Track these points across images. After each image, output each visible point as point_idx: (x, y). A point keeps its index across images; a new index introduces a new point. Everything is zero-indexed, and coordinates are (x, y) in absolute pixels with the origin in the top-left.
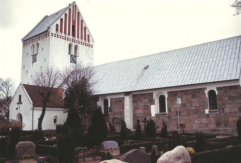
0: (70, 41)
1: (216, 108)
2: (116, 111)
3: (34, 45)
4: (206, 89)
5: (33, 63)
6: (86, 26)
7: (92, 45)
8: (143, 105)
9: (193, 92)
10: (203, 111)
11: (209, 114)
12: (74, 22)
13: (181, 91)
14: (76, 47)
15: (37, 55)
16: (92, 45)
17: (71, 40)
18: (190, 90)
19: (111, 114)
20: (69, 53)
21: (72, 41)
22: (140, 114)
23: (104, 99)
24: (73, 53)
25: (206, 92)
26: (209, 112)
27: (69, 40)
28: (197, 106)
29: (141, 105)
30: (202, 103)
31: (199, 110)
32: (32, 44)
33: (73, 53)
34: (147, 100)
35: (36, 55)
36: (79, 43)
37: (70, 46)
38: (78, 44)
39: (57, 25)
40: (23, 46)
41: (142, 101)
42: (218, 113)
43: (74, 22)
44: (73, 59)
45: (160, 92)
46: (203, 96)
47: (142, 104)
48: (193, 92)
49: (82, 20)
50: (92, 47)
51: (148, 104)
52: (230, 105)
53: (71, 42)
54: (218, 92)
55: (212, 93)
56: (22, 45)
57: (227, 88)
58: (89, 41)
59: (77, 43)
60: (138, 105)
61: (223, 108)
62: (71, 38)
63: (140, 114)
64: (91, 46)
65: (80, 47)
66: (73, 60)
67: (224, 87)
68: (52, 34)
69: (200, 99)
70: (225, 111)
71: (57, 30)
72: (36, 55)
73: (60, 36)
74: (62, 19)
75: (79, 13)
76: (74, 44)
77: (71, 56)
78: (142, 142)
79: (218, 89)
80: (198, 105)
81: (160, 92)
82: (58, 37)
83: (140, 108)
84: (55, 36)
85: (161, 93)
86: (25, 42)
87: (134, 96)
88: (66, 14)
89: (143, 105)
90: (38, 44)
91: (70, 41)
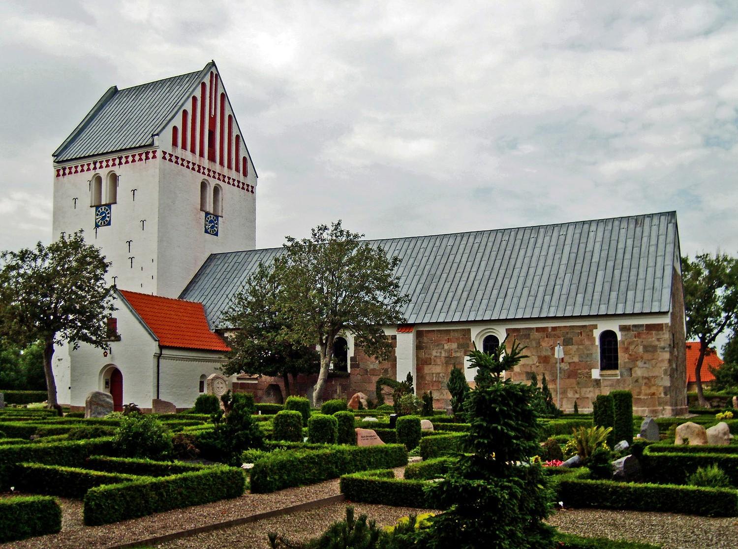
0: (204, 173)
1: (615, 367)
2: (372, 367)
3: (99, 180)
4: (595, 327)
5: (97, 226)
6: (239, 134)
7: (252, 187)
8: (443, 355)
9: (567, 333)
10: (587, 373)
11: (600, 380)
12: (213, 121)
13: (538, 329)
14: (216, 190)
15: (113, 206)
16: (252, 187)
17: (206, 172)
18: (559, 327)
19: (356, 372)
20: (202, 210)
21: (209, 175)
22: (434, 375)
23: (485, 336)
24: (210, 208)
25: (597, 334)
26: (601, 375)
27: (202, 171)
28: (574, 362)
29: (438, 354)
30: (584, 357)
31: (579, 371)
32: (92, 173)
33: (210, 208)
34: (454, 346)
35: (109, 205)
36: (224, 181)
37: (204, 186)
38: (221, 183)
39: (175, 129)
40: (58, 175)
41: (439, 345)
42: (619, 378)
43: (213, 121)
44: (212, 225)
45: (487, 329)
46: (587, 343)
47: (441, 353)
48: (567, 333)
49: (230, 117)
50: (252, 192)
51: (458, 354)
52: (645, 363)
53: (206, 177)
54: (622, 335)
55: (608, 337)
56: (53, 172)
57: (641, 329)
58: (245, 174)
59: (219, 179)
60: (431, 354)
61: (631, 369)
62: (207, 167)
63: (434, 375)
64: (250, 189)
65: (227, 190)
66: (106, 215)
67: (635, 326)
68: (165, 153)
69: (581, 347)
70: (634, 375)
71: (175, 144)
72: (109, 205)
73: (181, 159)
74: (185, 113)
75: (224, 96)
76: (213, 182)
77: (207, 214)
78: (439, 434)
79: (623, 328)
80: (576, 359)
81: (487, 329)
82: (177, 162)
83: (435, 361)
84: (170, 160)
85: (491, 330)
86: (60, 166)
87: (419, 335)
88: (195, 99)
89: (443, 355)
90: (114, 178)
91: (204, 173)
